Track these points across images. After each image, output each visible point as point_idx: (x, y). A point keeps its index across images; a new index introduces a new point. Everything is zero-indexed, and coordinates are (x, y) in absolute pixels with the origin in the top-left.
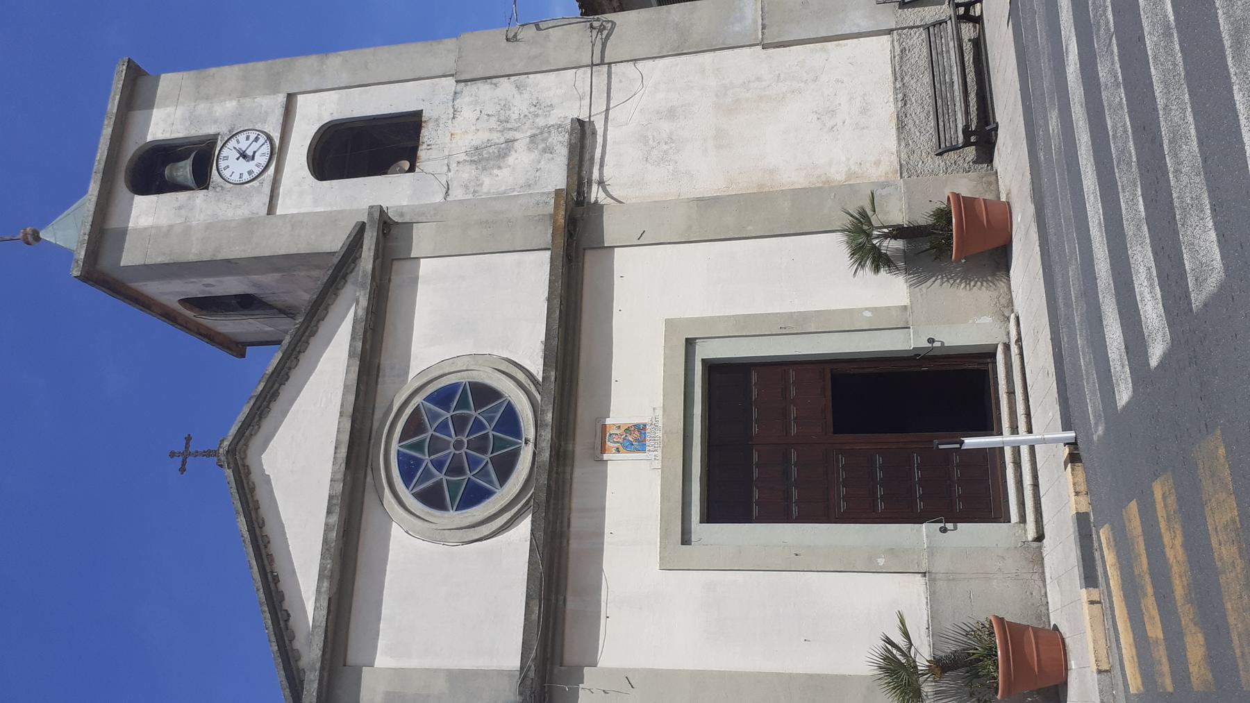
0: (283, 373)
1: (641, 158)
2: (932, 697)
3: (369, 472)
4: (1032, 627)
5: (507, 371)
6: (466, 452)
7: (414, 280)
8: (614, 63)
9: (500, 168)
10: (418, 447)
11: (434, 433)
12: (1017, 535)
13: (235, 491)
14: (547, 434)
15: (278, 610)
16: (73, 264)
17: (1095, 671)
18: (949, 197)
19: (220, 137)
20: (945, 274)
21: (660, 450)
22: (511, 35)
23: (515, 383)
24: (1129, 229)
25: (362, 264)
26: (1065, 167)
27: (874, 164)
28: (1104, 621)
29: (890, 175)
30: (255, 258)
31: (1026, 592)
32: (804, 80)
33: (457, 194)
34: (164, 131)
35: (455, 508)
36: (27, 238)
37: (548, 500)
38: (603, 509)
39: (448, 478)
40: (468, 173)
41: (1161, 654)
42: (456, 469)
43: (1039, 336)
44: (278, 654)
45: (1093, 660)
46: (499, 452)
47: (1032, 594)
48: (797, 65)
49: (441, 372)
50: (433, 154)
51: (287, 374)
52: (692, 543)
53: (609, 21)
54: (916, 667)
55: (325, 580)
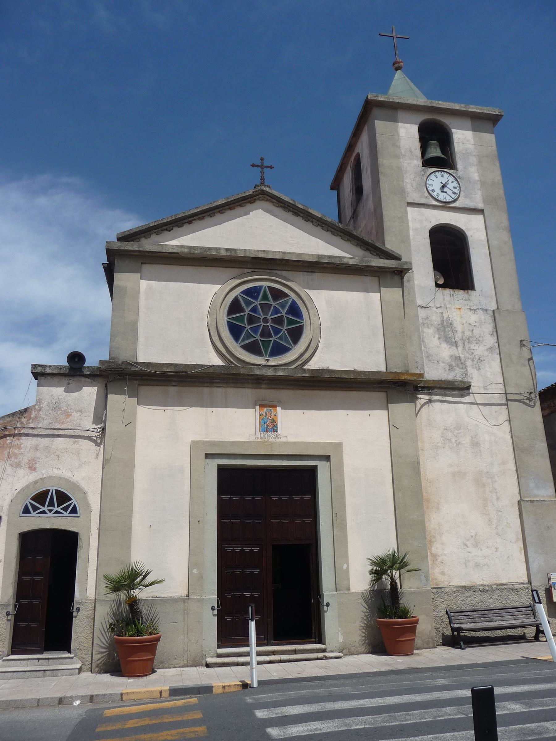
0: (309, 218)
1: (447, 426)
2: (118, 598)
3: (251, 270)
4: (154, 658)
5: (310, 347)
6: (261, 325)
7: (366, 290)
8: (508, 408)
9: (439, 338)
10: (265, 297)
11: (273, 306)
12: (210, 652)
13: (240, 196)
14: (270, 372)
15: (172, 225)
16: (375, 94)
17: (122, 692)
18: (416, 617)
19: (456, 171)
20: (370, 614)
21: (261, 440)
22: (524, 343)
23: (302, 352)
24: (348, 721)
25: (375, 260)
26: (410, 687)
27: (442, 571)
28: (150, 699)
29: (435, 582)
30: (380, 197)
31: (176, 656)
32: (498, 527)
33: (422, 313)
34: (459, 138)
35: (228, 320)
36: (396, 64)
37: (231, 374)
38: (226, 406)
39: (246, 315)
40: (436, 319)
41: (118, 726)
42: (251, 320)
43: (323, 670)
44: (148, 227)
45: (129, 691)
46: (261, 344)
47: (175, 659)
48: (507, 523)
49: (309, 308)
50: (447, 298)
51: (309, 220)
52: (206, 460)
53: (535, 403)
54: (133, 589)
55: (188, 250)
